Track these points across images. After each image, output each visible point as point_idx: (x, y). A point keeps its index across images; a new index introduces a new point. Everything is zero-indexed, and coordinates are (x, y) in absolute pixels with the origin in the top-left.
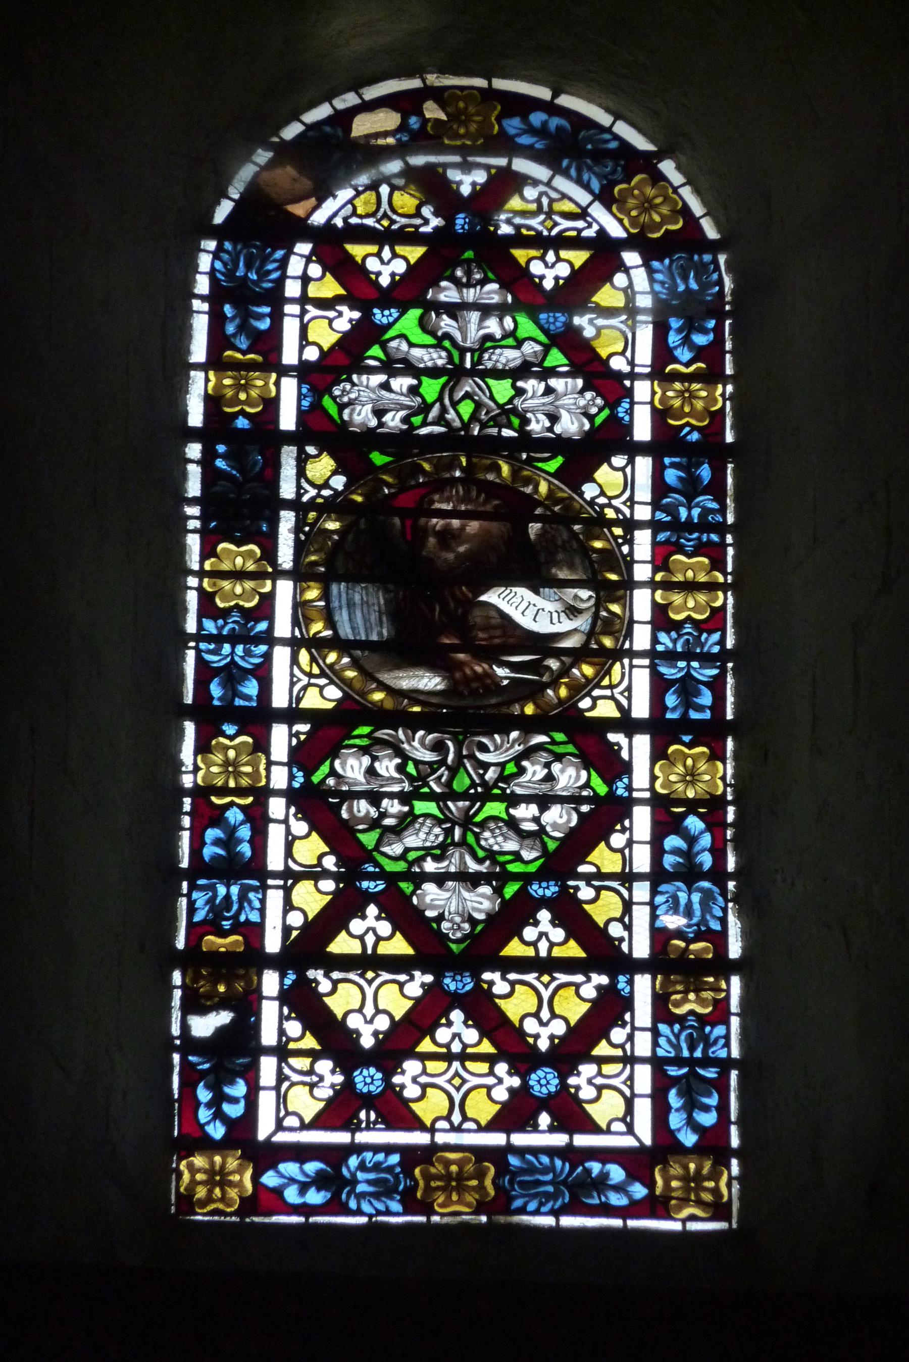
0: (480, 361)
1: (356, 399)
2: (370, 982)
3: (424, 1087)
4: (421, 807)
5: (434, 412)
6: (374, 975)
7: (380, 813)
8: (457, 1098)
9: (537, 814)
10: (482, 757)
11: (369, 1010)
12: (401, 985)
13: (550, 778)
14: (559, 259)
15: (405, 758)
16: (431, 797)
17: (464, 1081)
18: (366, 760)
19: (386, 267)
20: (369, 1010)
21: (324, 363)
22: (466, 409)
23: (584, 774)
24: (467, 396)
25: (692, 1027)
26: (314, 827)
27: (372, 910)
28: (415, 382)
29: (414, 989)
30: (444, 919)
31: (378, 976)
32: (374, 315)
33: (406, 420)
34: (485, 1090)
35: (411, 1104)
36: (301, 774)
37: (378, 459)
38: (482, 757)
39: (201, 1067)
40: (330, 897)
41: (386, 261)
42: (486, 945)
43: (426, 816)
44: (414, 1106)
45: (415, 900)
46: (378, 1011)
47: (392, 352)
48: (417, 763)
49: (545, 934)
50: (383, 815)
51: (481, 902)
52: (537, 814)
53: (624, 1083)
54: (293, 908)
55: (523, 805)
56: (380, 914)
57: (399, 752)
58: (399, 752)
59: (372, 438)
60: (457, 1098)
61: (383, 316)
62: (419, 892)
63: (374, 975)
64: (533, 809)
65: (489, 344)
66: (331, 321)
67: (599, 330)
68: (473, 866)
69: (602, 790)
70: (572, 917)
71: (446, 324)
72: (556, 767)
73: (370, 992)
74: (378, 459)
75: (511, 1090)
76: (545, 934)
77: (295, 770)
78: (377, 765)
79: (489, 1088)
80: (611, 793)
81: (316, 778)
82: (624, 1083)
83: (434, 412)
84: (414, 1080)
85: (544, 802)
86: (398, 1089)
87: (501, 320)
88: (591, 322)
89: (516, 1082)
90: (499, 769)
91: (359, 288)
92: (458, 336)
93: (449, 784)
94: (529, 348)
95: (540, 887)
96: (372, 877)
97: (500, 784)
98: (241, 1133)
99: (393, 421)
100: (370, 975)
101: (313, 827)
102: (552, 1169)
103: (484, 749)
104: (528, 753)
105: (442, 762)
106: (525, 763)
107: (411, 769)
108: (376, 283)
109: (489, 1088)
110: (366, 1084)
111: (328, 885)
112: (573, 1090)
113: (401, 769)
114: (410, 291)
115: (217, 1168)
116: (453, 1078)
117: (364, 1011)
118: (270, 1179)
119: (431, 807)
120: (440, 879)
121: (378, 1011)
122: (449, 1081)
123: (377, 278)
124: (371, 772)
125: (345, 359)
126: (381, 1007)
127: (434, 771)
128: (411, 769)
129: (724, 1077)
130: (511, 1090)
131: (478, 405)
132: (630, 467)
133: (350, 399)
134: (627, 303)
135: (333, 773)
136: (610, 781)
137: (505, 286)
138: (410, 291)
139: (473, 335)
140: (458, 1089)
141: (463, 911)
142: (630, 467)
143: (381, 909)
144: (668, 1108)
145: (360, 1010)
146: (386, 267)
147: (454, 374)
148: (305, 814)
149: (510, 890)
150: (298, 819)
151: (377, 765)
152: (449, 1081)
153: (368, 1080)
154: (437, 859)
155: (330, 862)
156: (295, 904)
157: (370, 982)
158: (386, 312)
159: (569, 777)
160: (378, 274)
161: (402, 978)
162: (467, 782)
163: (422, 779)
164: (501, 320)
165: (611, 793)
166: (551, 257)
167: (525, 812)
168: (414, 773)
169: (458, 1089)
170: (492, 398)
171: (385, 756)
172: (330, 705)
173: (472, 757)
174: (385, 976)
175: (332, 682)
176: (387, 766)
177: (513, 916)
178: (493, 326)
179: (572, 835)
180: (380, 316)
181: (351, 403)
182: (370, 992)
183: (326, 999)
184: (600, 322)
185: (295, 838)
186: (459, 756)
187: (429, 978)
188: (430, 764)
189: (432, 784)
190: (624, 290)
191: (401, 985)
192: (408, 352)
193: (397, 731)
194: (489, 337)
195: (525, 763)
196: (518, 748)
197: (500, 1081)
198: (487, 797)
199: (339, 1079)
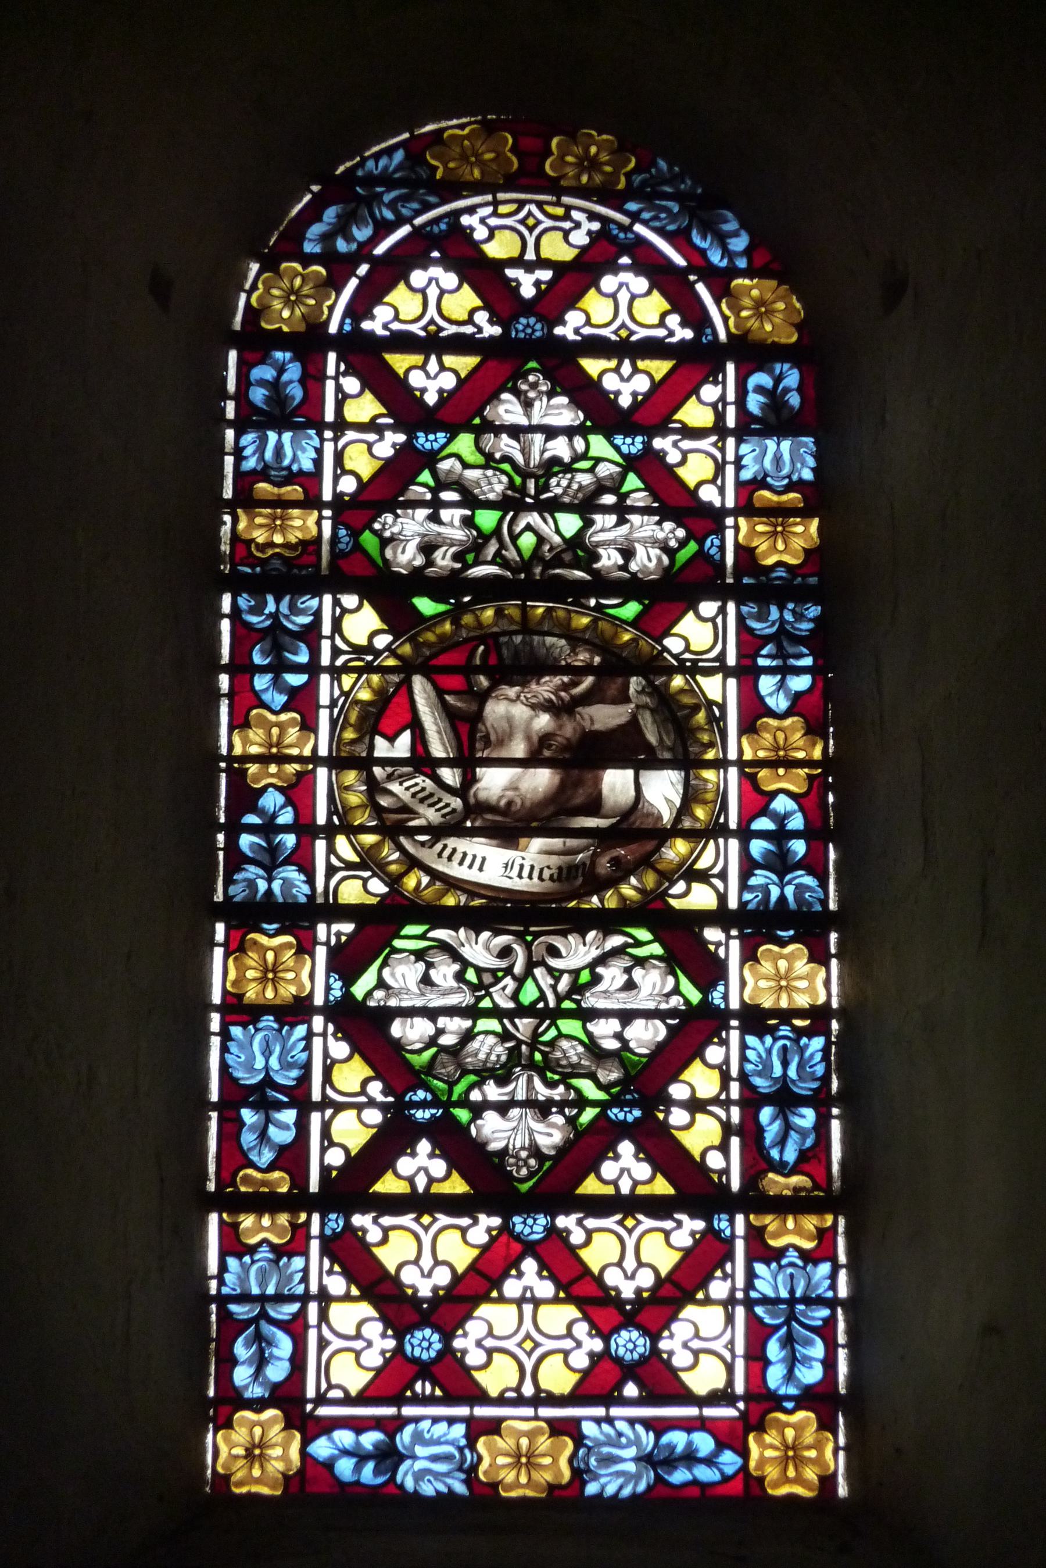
0: (546, 488)
1: (400, 533)
2: (426, 1229)
3: (490, 1352)
4: (483, 1024)
5: (492, 548)
6: (431, 1219)
7: (437, 1029)
8: (529, 1366)
9: (618, 1029)
10: (553, 963)
11: (427, 1261)
12: (464, 1231)
13: (630, 986)
14: (636, 370)
15: (465, 964)
16: (496, 1012)
17: (537, 1345)
18: (421, 966)
19: (432, 381)
20: (427, 1261)
21: (360, 498)
22: (527, 541)
23: (671, 980)
24: (528, 528)
25: (792, 1265)
26: (356, 1048)
27: (424, 1146)
28: (468, 512)
29: (479, 1235)
30: (508, 1154)
31: (435, 1220)
32: (417, 438)
33: (456, 557)
34: (561, 1356)
35: (473, 1372)
36: (716, 1002)
37: (426, 606)
38: (553, 963)
39: (831, 751)
40: (375, 1130)
41: (432, 375)
42: (559, 1183)
43: (487, 1033)
44: (477, 1375)
45: (473, 1132)
46: (437, 1263)
47: (442, 476)
48: (479, 971)
49: (626, 1168)
50: (440, 1032)
51: (551, 1135)
52: (618, 1029)
53: (726, 1347)
54: (332, 1144)
55: (602, 1021)
56: (433, 1151)
57: (455, 956)
58: (455, 956)
59: (419, 581)
60: (529, 1366)
61: (427, 440)
62: (479, 1122)
63: (431, 1219)
64: (614, 1025)
65: (556, 469)
66: (667, 1234)
67: (685, 454)
68: (543, 1092)
69: (695, 996)
70: (662, 1149)
71: (507, 445)
72: (638, 974)
73: (427, 1239)
74: (426, 606)
75: (591, 1355)
76: (626, 1168)
77: (722, 1006)
78: (432, 972)
79: (566, 1353)
80: (705, 1002)
81: (359, 990)
82: (726, 1347)
83: (492, 548)
84: (479, 1344)
85: (626, 1017)
86: (459, 1355)
87: (571, 440)
88: (675, 444)
89: (597, 1345)
90: (481, 558)
91: (403, 407)
92: (519, 459)
93: (515, 997)
94: (605, 470)
95: (622, 1110)
96: (423, 1105)
97: (840, 1311)
98: (287, 1398)
99: (444, 560)
100: (426, 1219)
101: (355, 1049)
102: (637, 1442)
103: (554, 952)
104: (602, 960)
105: (509, 971)
106: (600, 970)
107: (471, 975)
108: (421, 402)
109: (566, 1353)
110: (424, 1339)
111: (374, 1116)
112: (665, 1356)
113: (460, 977)
114: (464, 410)
115: (257, 1440)
116: (524, 1340)
117: (421, 1263)
118: (321, 1448)
119: (493, 1024)
120: (503, 1108)
121: (437, 1263)
122: (519, 1345)
123: (422, 394)
124: (426, 980)
125: (387, 490)
126: (440, 1258)
127: (498, 980)
128: (471, 975)
129: (830, 1323)
130: (591, 1355)
131: (541, 539)
132: (720, 617)
133: (392, 533)
134: (716, 423)
135: (381, 984)
136: (705, 986)
137: (576, 402)
138: (464, 410)
139: (538, 458)
140: (529, 1354)
141: (530, 1145)
142: (720, 617)
143: (435, 1144)
144: (767, 1363)
145: (416, 1262)
146: (432, 381)
147: (511, 504)
148: (345, 1033)
149: (589, 1115)
150: (337, 1039)
151: (432, 972)
152: (519, 1345)
153: (424, 1343)
154: (502, 1081)
155: (375, 1089)
156: (336, 1140)
157: (426, 1229)
158: (431, 437)
159: (652, 983)
160: (423, 390)
161: (465, 1221)
162: (536, 994)
163: (481, 988)
164: (571, 440)
165: (705, 1002)
166: (626, 368)
167: (604, 1030)
168: (475, 980)
169: (529, 1354)
170: (558, 531)
171: (441, 963)
172: (374, 901)
173: (543, 963)
174: (443, 1220)
175: (375, 875)
176: (444, 972)
177: (588, 1147)
178: (560, 448)
179: (660, 1049)
180: (424, 441)
181: (392, 539)
182: (427, 1239)
183: (375, 1250)
184: (686, 444)
185: (334, 1062)
186: (531, 965)
187: (496, 1221)
188: (493, 972)
189: (496, 996)
190: (714, 406)
191: (464, 1231)
192: (461, 475)
193: (457, 932)
194: (555, 461)
195: (600, 970)
196: (595, 953)
197: (579, 1344)
198: (555, 1014)
199: (391, 1344)
